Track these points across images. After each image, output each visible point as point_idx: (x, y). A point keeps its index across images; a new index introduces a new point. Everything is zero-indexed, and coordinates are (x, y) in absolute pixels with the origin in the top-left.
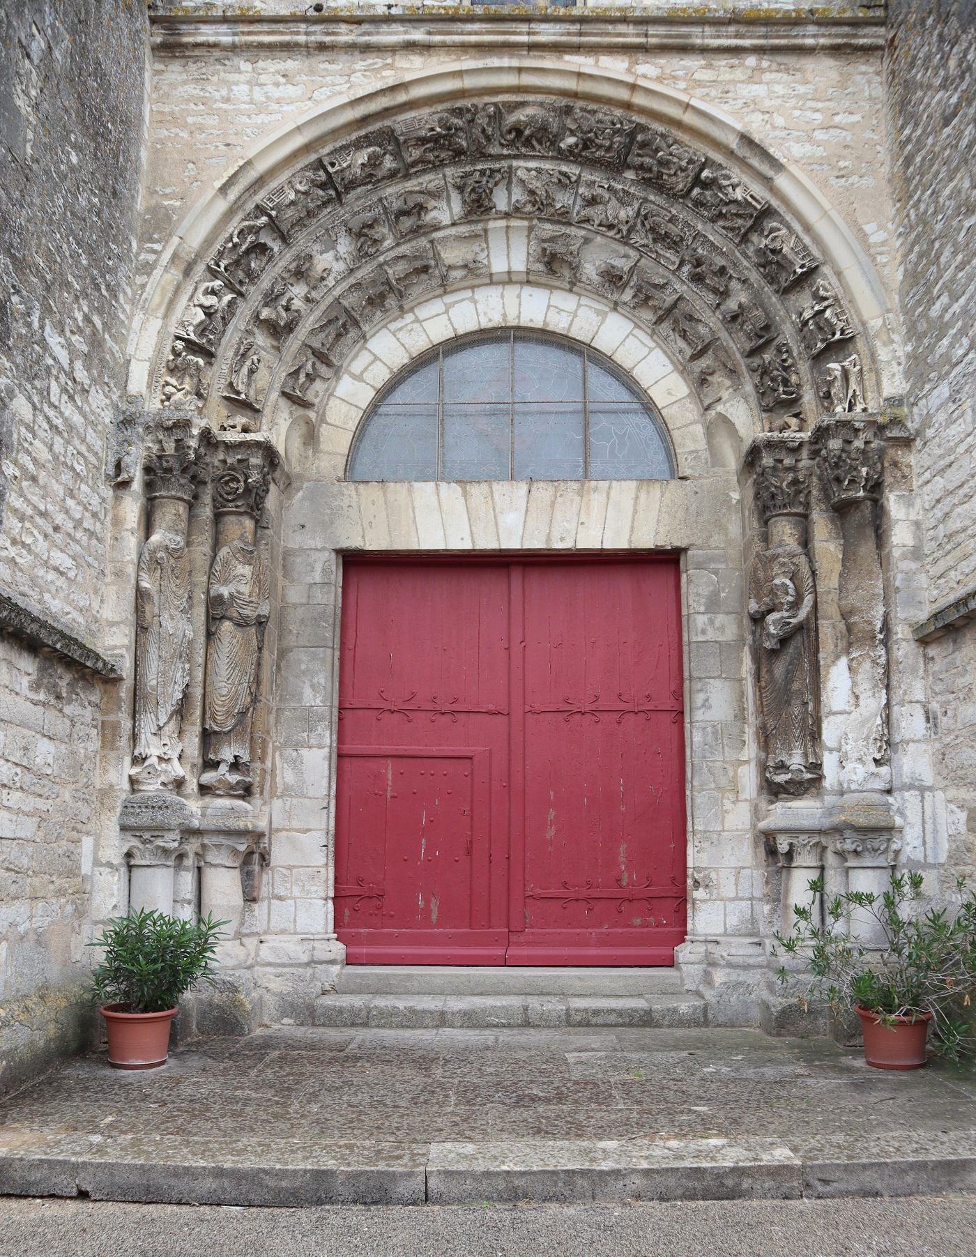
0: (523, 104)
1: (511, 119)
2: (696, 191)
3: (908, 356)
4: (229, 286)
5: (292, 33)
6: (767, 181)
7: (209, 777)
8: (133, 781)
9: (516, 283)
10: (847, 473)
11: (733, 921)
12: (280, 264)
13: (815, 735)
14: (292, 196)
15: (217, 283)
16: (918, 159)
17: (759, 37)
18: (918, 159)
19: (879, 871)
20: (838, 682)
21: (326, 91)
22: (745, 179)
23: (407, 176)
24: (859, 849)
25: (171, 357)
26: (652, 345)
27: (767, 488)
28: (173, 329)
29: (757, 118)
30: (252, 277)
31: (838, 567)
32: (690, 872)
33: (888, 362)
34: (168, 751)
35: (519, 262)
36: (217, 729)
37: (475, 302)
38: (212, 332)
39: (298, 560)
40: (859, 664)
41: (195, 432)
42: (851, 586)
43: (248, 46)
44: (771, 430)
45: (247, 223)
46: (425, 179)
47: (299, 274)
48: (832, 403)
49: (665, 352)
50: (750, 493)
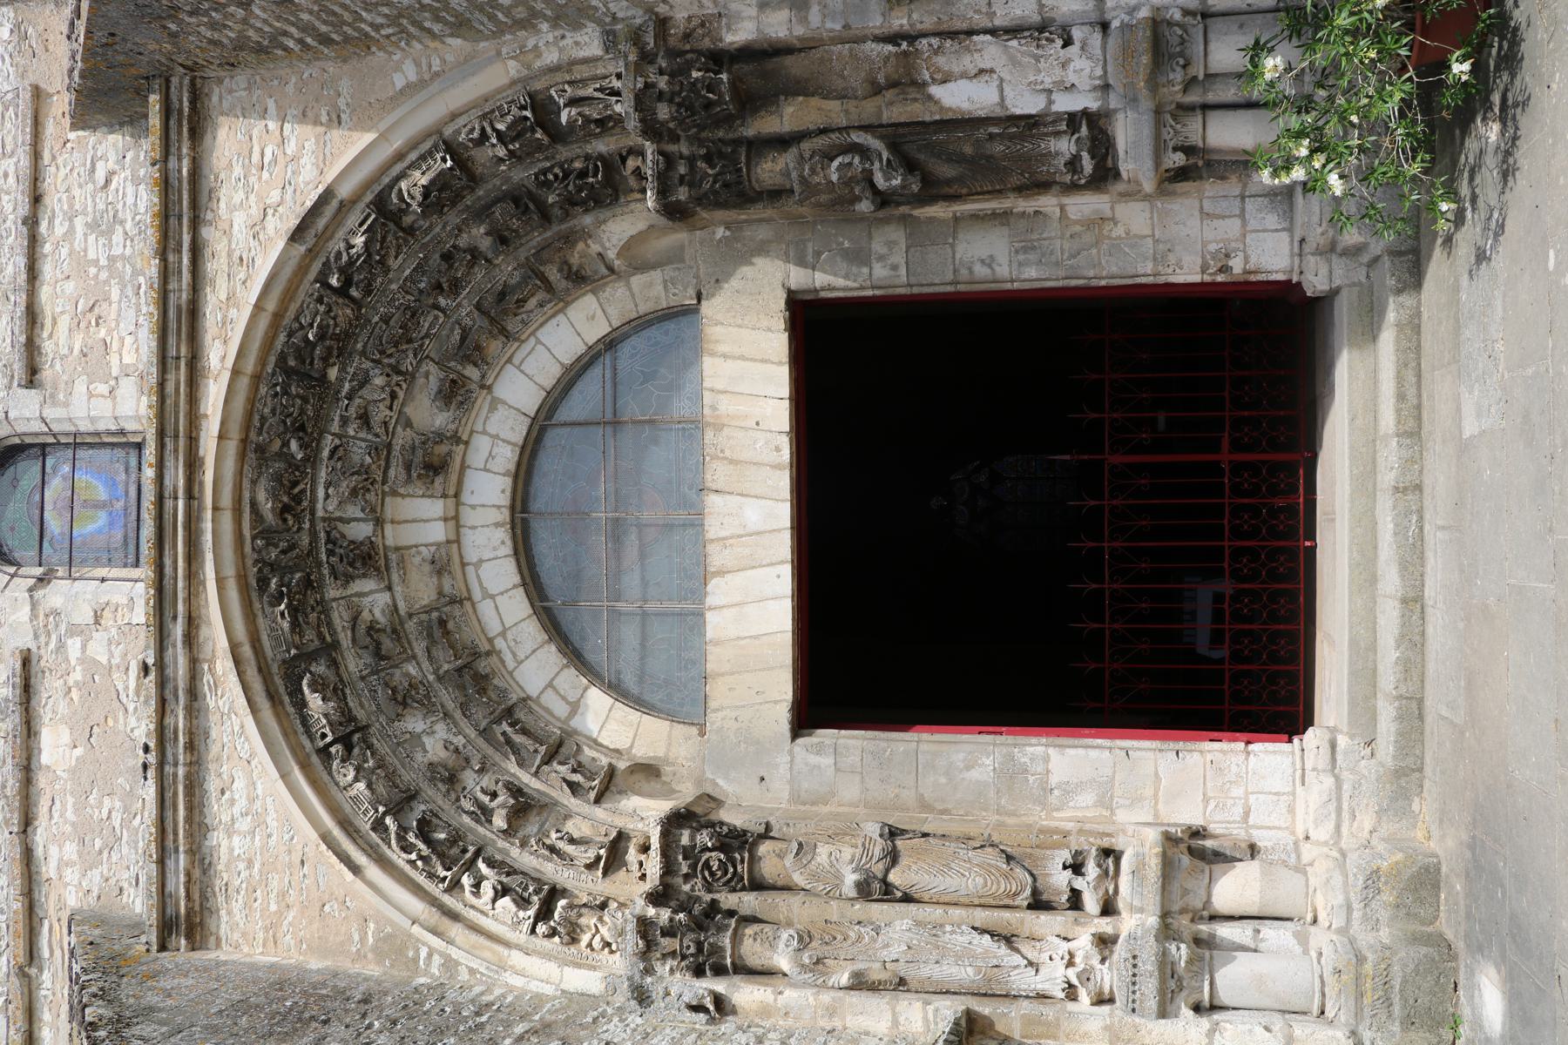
1: (270, 518)
2: (354, 293)
3: (555, 26)
4: (470, 866)
5: (175, 782)
6: (345, 207)
7: (1091, 903)
8: (1102, 1000)
9: (457, 511)
10: (697, 93)
11: (1272, 220)
12: (440, 802)
13: (1031, 123)
14: (361, 786)
15: (466, 880)
16: (324, 28)
17: (180, 224)
18: (324, 28)
19: (1211, 36)
20: (961, 96)
22: (341, 234)
23: (336, 645)
24: (1182, 62)
25: (556, 939)
26: (532, 340)
27: (716, 193)
28: (521, 937)
29: (271, 223)
30: (456, 838)
31: (815, 101)
32: (1207, 278)
33: (561, 50)
34: (1058, 949)
35: (434, 508)
36: (1028, 892)
37: (481, 561)
38: (526, 889)
39: (805, 785)
40: (939, 70)
41: (651, 911)
42: (839, 84)
43: (190, 835)
44: (644, 191)
45: (393, 842)
46: (337, 621)
47: (452, 779)
48: (610, 117)
49: (542, 325)
50: (720, 214)
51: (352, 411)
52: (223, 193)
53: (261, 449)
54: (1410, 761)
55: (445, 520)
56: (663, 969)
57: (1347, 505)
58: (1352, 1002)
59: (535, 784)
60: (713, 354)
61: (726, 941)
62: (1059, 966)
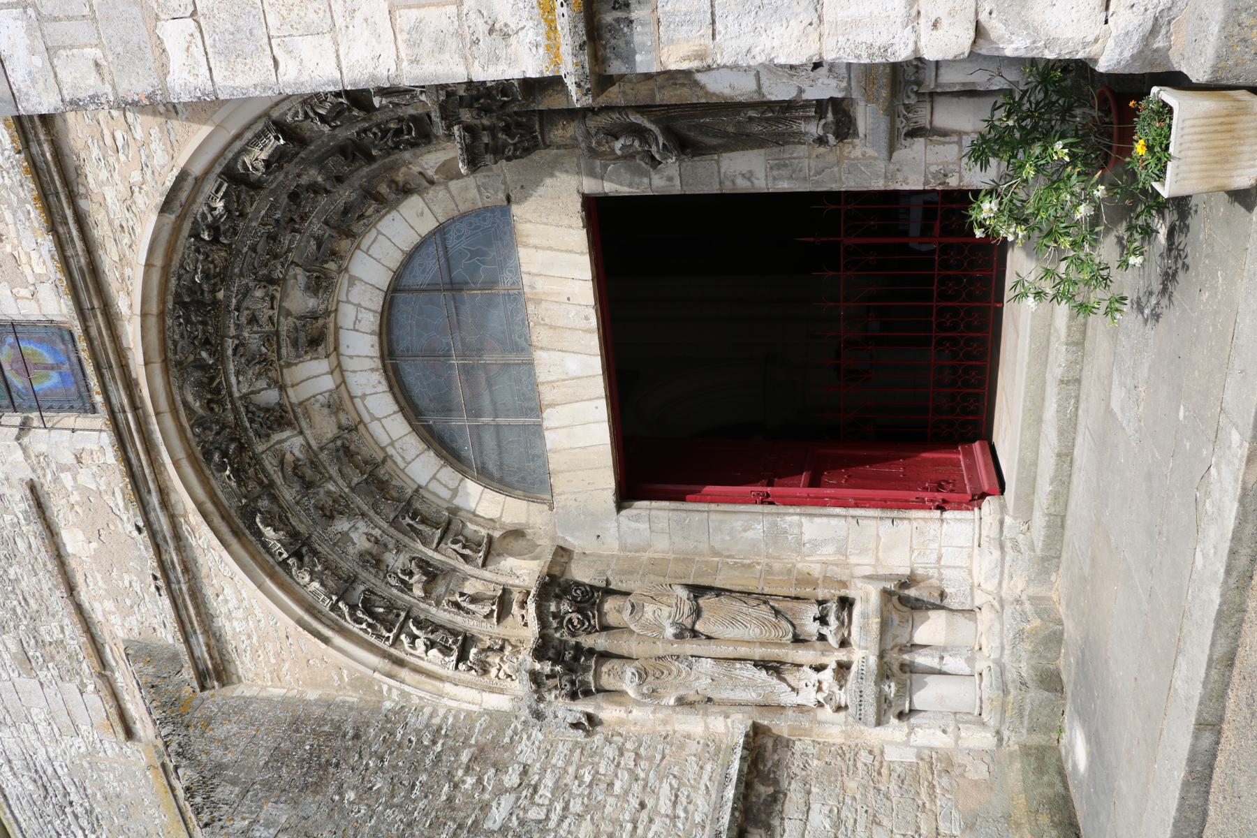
0: (185, 403)
6: (200, 181)
7: (833, 641)
14: (316, 585)
21: (221, 567)
22: (201, 199)
23: (272, 484)
28: (449, 671)
29: (140, 199)
30: (391, 606)
36: (790, 635)
38: (447, 641)
41: (538, 666)
43: (201, 622)
46: (269, 467)
51: (243, 320)
52: (88, 169)
53: (179, 364)
54: (1052, 553)
55: (332, 373)
56: (550, 697)
57: (1025, 369)
58: (998, 716)
59: (436, 556)
60: (526, 246)
61: (590, 677)
62: (813, 690)
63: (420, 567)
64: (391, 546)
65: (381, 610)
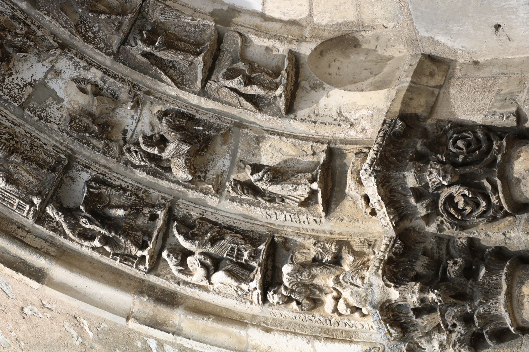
12: (103, 161)
28: (253, 307)
30: (139, 202)
38: (240, 255)
41: (394, 294)
45: (68, 232)
63: (177, 128)
64: (124, 96)
65: (120, 212)
